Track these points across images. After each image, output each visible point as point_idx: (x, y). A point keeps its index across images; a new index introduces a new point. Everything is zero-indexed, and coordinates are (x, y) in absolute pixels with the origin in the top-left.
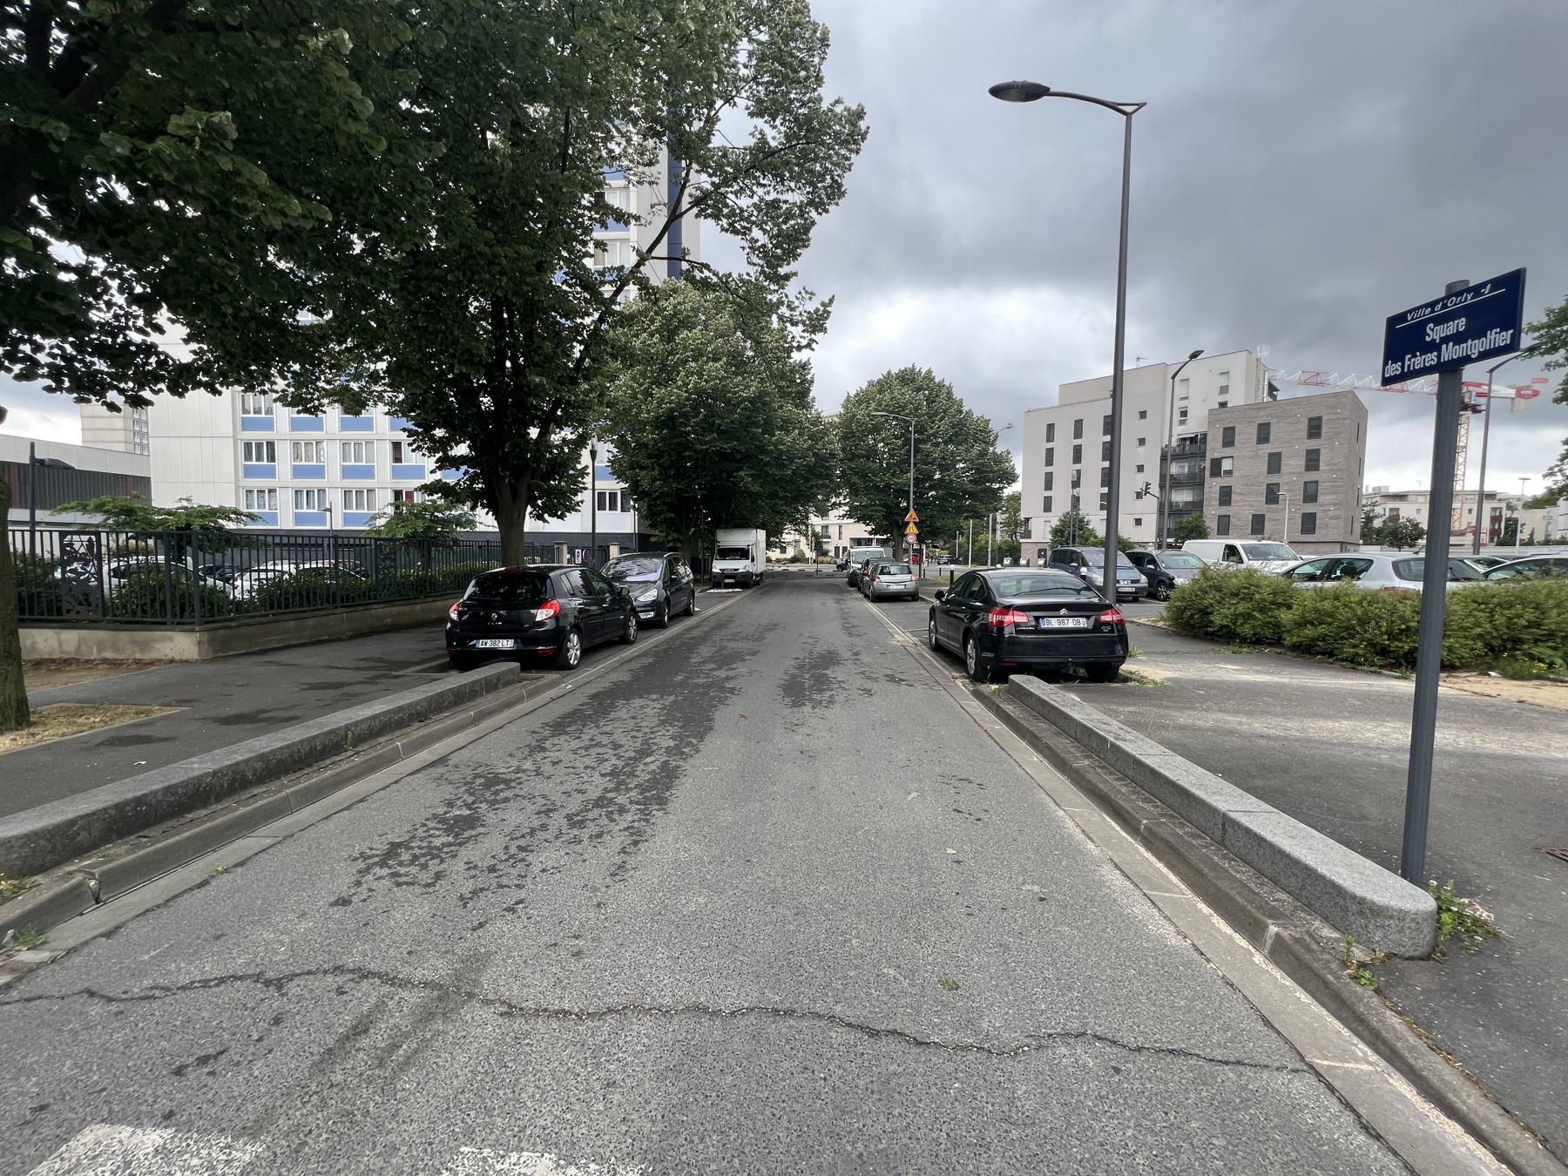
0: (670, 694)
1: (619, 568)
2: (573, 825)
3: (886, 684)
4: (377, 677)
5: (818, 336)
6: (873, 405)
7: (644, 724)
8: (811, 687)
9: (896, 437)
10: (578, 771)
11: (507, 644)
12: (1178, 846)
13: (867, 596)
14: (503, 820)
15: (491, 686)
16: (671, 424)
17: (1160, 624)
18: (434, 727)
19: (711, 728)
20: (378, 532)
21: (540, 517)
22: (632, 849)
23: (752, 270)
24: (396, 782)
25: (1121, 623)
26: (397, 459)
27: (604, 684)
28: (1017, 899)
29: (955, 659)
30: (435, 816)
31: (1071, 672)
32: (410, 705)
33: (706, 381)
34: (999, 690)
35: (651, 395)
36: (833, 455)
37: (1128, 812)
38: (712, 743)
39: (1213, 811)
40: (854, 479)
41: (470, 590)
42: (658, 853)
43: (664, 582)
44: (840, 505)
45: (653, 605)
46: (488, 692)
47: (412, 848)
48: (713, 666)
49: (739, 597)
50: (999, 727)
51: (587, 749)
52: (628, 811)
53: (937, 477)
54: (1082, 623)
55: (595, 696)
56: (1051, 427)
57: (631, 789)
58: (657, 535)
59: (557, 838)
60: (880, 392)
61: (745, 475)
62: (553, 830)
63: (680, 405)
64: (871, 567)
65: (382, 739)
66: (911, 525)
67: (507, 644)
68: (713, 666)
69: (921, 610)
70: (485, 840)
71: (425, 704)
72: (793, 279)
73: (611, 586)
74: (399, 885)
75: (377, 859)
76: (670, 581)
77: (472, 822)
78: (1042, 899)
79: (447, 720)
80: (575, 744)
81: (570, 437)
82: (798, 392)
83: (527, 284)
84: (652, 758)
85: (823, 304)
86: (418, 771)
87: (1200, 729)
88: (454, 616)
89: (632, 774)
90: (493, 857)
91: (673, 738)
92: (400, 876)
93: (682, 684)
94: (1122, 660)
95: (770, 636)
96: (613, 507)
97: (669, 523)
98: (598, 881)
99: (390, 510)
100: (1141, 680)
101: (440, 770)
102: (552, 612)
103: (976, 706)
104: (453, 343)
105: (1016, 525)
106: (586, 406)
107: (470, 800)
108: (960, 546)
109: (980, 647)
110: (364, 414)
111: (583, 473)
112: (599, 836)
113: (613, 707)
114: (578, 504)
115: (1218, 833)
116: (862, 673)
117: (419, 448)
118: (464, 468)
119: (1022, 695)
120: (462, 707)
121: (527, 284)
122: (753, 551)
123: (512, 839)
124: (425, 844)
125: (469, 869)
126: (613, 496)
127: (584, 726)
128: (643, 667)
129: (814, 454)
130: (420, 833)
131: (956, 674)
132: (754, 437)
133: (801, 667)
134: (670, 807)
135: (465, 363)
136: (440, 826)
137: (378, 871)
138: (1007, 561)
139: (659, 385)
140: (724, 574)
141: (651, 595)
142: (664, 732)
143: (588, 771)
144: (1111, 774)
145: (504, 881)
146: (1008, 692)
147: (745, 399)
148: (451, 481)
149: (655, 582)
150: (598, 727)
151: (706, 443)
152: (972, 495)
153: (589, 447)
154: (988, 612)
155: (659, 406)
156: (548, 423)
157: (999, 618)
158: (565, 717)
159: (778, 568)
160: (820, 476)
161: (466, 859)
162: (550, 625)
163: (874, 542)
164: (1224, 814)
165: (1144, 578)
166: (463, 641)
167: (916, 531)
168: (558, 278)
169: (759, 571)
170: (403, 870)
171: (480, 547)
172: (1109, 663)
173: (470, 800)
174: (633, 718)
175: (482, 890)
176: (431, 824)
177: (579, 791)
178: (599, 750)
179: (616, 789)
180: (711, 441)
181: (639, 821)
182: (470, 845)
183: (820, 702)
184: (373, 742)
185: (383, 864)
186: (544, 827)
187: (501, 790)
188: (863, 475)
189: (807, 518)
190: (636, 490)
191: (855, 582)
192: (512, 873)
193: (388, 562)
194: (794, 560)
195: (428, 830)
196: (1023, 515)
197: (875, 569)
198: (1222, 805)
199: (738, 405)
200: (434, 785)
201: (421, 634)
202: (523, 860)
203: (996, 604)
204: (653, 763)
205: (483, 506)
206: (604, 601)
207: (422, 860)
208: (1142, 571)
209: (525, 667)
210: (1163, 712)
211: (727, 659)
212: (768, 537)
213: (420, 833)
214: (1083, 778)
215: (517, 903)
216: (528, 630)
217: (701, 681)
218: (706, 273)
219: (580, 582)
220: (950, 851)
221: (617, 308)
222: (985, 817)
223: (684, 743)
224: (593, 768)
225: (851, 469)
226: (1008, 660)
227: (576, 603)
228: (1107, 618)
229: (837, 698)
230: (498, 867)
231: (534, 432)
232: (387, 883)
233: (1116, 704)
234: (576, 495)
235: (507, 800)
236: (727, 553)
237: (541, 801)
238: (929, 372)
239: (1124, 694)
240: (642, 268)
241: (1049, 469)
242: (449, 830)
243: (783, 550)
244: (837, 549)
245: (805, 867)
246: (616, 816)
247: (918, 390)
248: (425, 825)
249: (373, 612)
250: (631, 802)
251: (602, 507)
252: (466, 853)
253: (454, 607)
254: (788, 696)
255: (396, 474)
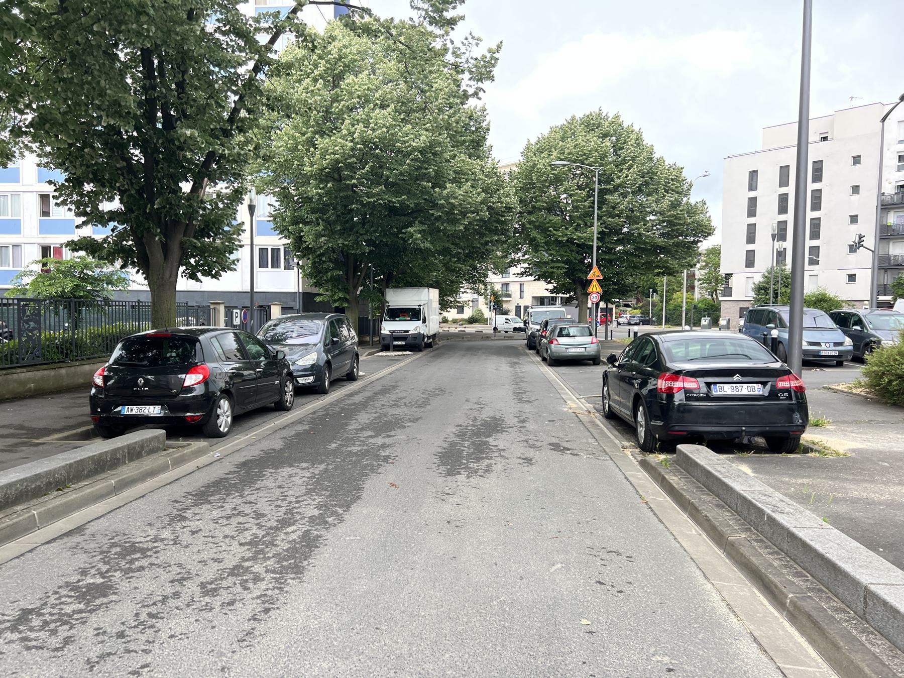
0: (321, 462)
1: (279, 329)
2: (205, 593)
3: (549, 453)
4: (16, 445)
5: (486, 85)
6: (555, 153)
7: (290, 493)
8: (469, 455)
9: (580, 188)
10: (217, 540)
11: (154, 411)
12: (820, 620)
13: (544, 359)
14: (136, 588)
15: (134, 453)
16: (336, 175)
17: (859, 391)
18: (72, 495)
19: (359, 498)
20: (24, 291)
21: (193, 276)
22: (263, 616)
23: (415, 15)
24: (31, 551)
25: (800, 390)
26: (46, 213)
27: (254, 452)
28: (644, 670)
29: (626, 427)
30: (67, 584)
31: (745, 441)
32: (48, 473)
33: (373, 130)
34: (665, 460)
35: (314, 146)
36: (509, 209)
37: (776, 586)
38: (359, 511)
39: (855, 583)
40: (534, 234)
41: (117, 352)
42: (287, 620)
43: (325, 345)
44: (519, 261)
45: (313, 369)
46: (131, 460)
47: (43, 614)
48: (370, 433)
49: (409, 360)
50: (665, 499)
51: (228, 518)
52: (263, 579)
53: (625, 230)
54: (757, 390)
55: (244, 464)
56: (753, 174)
57: (269, 558)
58: (323, 294)
59: (188, 605)
60: (563, 139)
61: (415, 232)
62: (185, 598)
63: (346, 156)
64: (549, 328)
65: (19, 508)
66: (595, 283)
67: (154, 411)
68: (370, 433)
69: (597, 372)
70: (117, 607)
71: (63, 473)
72: (460, 23)
73: (266, 350)
74: (28, 648)
75: (8, 624)
76: (333, 344)
77: (104, 590)
78: (670, 670)
79: (87, 488)
80: (216, 514)
81: (224, 191)
82: (472, 141)
83: (177, 34)
84: (294, 528)
85: (490, 51)
86: (54, 540)
87: (873, 503)
88: (99, 381)
89: (272, 544)
90: (123, 624)
91: (318, 507)
92: (30, 640)
93: (335, 453)
94: (802, 428)
95: (435, 403)
96: (276, 264)
97: (335, 282)
98: (225, 646)
99: (37, 268)
100: (823, 451)
101: (77, 539)
102: (200, 377)
103: (642, 477)
104: (100, 95)
105: (717, 281)
106: (240, 160)
107: (104, 568)
108: (654, 305)
109: (649, 416)
110: (10, 165)
111: (239, 230)
112: (231, 603)
113: (260, 476)
114: (233, 262)
115: (861, 606)
116: (526, 441)
117: (64, 203)
118: (112, 224)
119: (689, 466)
120: (103, 476)
121: (177, 34)
122: (425, 312)
123: (143, 607)
124: (56, 611)
125: (98, 635)
126: (276, 251)
127: (228, 495)
128: (297, 435)
129: (489, 208)
130: (52, 600)
131: (627, 444)
132: (424, 191)
133: (462, 435)
134: (306, 576)
135: (113, 116)
136: (72, 593)
137: (9, 635)
138: (705, 321)
139: (322, 134)
140: (395, 336)
141: (310, 359)
142: (309, 501)
143: (227, 540)
144: (766, 547)
145: (132, 646)
146: (676, 462)
147: (414, 149)
148: (99, 237)
149: (315, 345)
150: (242, 496)
151: (373, 196)
152: (664, 249)
153: (246, 202)
154: (657, 377)
155: (323, 156)
156: (202, 175)
157: (669, 384)
158: (208, 486)
159: (454, 329)
160: (496, 232)
161: (95, 626)
162: (199, 390)
163: (559, 301)
164: (866, 588)
165: (848, 342)
166: (108, 406)
167: (599, 289)
168: (210, 24)
169: (432, 333)
170: (33, 635)
171: (133, 307)
172: (787, 433)
173: (104, 568)
174: (280, 487)
175: (109, 654)
176: (64, 592)
177: (215, 560)
178: (241, 519)
179: (254, 558)
180: (378, 194)
181: (274, 588)
182: (100, 612)
183: (476, 471)
184: (9, 511)
185: (14, 629)
186: (176, 595)
187: (137, 559)
188: (542, 228)
189: (486, 276)
190: (299, 246)
191: (533, 344)
192: (139, 639)
193: (32, 324)
194: (472, 321)
195: (59, 598)
196: (723, 271)
197: (553, 331)
198: (864, 577)
199: (408, 154)
200: (69, 553)
201: (65, 400)
202: (152, 627)
203: (668, 369)
204: (294, 533)
205: (133, 264)
206: (258, 365)
207: (53, 626)
208: (845, 333)
209: (172, 434)
210: (837, 484)
211: (385, 426)
212: (442, 295)
213: (52, 600)
214: (738, 551)
215: (143, 667)
216: (176, 395)
217: (355, 449)
218: (367, 19)
219: (234, 346)
220: (584, 622)
221: (272, 56)
222: (627, 589)
223: (329, 513)
224: (233, 537)
225: (530, 222)
226: (679, 428)
227: (228, 368)
228: (783, 384)
229: (494, 467)
230: (127, 633)
231: (186, 187)
232: (17, 646)
233: (790, 476)
234: (231, 253)
235: (142, 568)
236: (396, 314)
237: (175, 570)
238: (617, 116)
239: (801, 465)
240: (299, 14)
241: (752, 220)
242: (81, 597)
243: (461, 310)
244: (518, 308)
245: (434, 635)
246: (250, 585)
247: (605, 136)
248: (56, 593)
249: (15, 376)
250: (267, 571)
251: (263, 264)
252: (94, 620)
253: (99, 371)
254: (444, 464)
255: (44, 229)
